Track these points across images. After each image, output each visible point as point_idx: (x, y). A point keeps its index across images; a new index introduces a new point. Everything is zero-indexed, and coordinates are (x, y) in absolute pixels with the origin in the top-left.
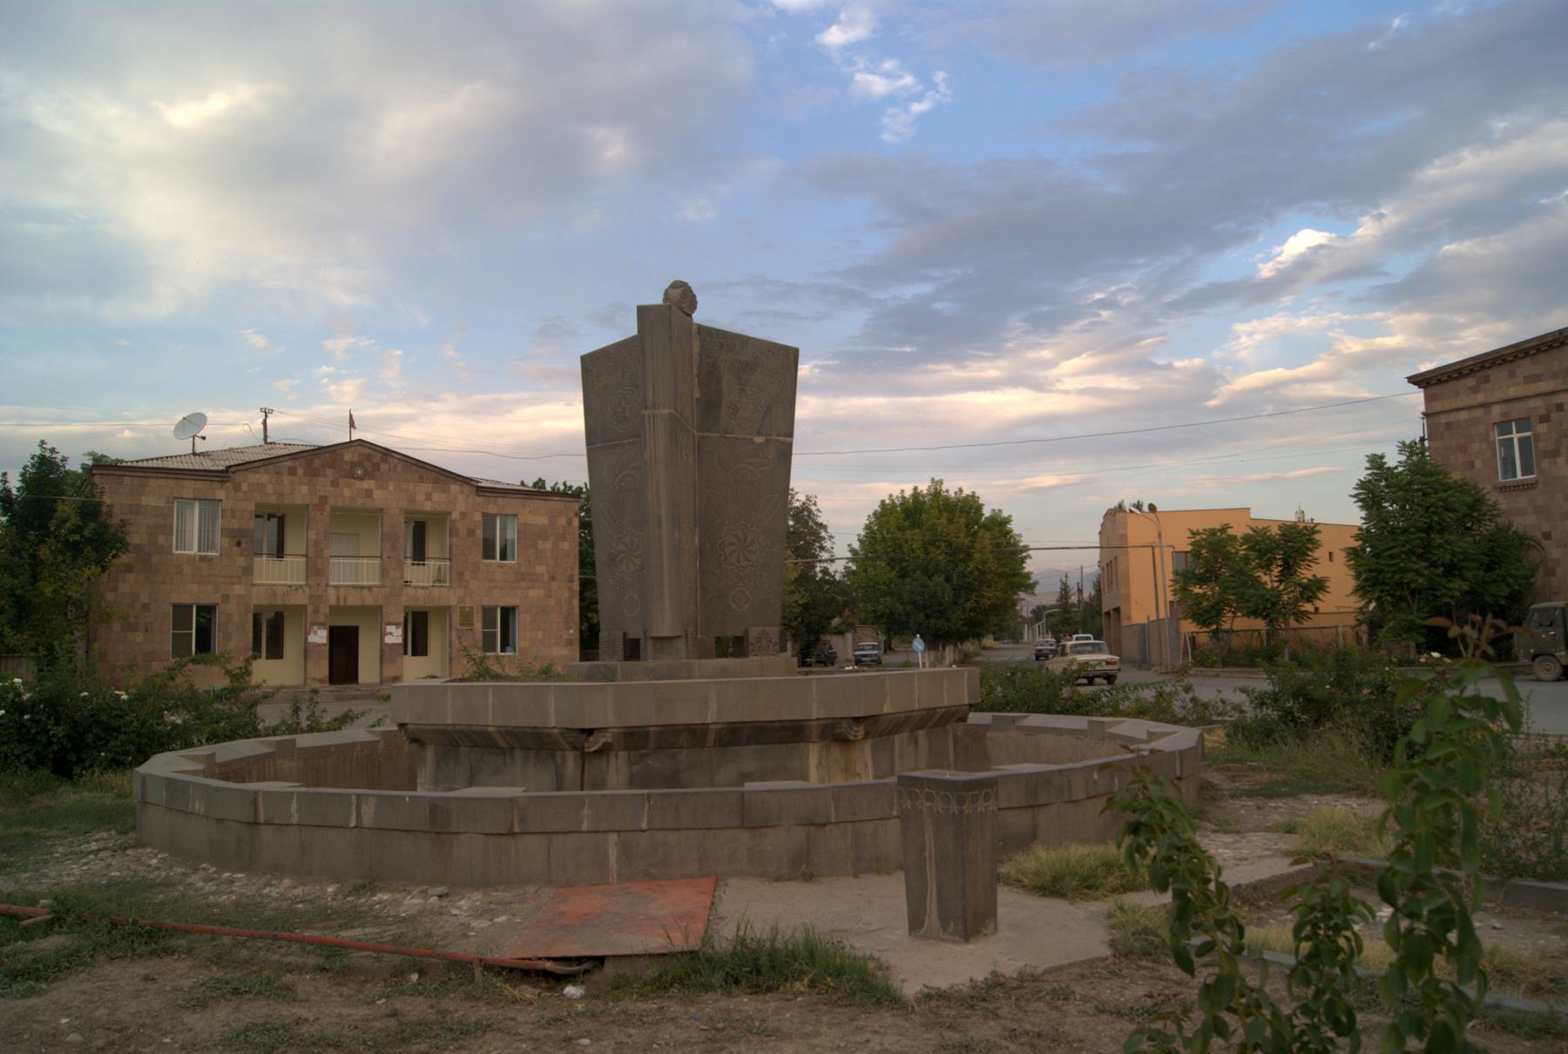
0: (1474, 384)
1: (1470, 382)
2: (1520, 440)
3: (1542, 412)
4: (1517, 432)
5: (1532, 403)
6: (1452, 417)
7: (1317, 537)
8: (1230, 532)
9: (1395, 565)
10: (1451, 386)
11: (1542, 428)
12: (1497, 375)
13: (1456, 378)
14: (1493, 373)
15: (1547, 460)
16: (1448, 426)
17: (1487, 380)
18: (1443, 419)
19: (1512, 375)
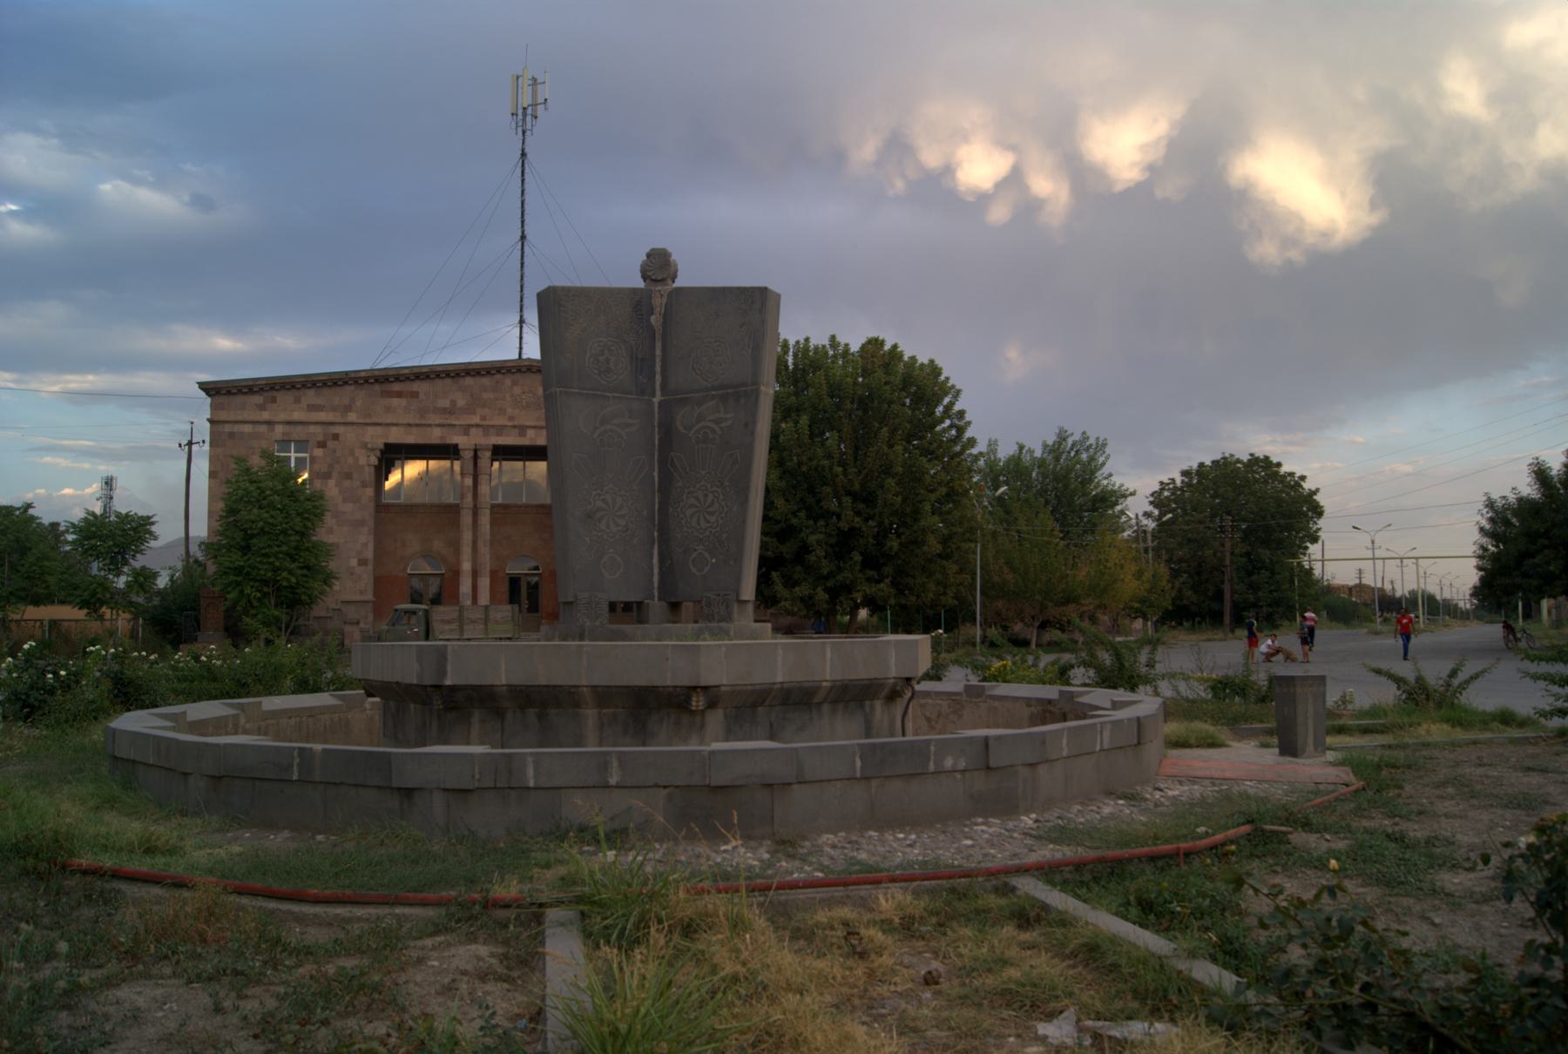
0: (261, 402)
1: (258, 399)
2: (296, 458)
3: (321, 438)
4: (295, 452)
5: (312, 429)
6: (237, 428)
7: (153, 528)
8: (31, 511)
9: (270, 563)
10: (239, 399)
11: (319, 452)
12: (285, 398)
13: (246, 393)
14: (280, 395)
15: (319, 481)
16: (232, 435)
17: (274, 400)
18: (227, 428)
19: (297, 401)
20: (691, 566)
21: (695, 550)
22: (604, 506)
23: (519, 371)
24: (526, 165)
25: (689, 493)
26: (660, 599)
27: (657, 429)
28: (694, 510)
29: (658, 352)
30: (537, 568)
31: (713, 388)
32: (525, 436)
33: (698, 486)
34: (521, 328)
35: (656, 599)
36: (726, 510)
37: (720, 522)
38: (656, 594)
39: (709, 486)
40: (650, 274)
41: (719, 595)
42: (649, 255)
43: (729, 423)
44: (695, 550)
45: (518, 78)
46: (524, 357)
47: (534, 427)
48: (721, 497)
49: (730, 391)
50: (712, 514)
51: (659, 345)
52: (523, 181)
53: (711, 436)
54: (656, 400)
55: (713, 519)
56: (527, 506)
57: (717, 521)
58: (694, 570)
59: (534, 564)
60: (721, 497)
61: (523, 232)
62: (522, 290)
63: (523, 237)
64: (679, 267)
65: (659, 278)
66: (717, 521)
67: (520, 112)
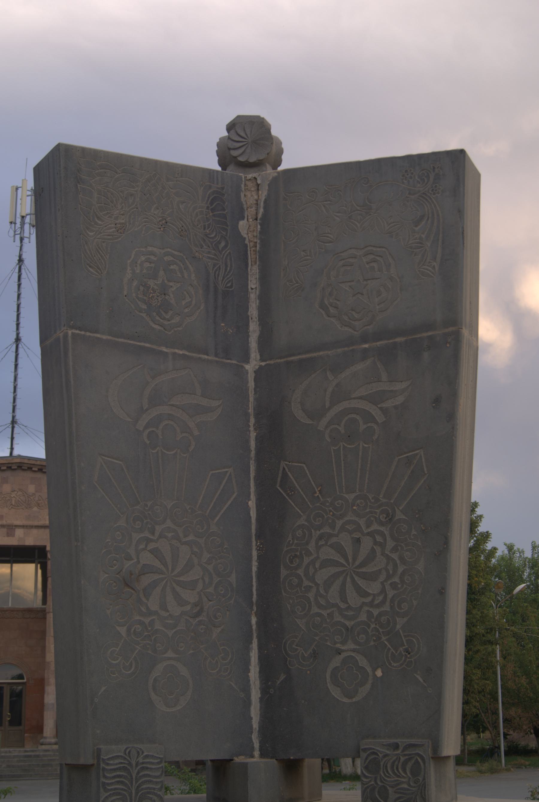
20: (330, 686)
21: (339, 652)
22: (157, 564)
23: (9, 468)
24: (23, 271)
25: (320, 537)
26: (263, 755)
27: (252, 421)
28: (333, 570)
29: (253, 283)
30: (21, 677)
31: (364, 339)
32: (13, 535)
33: (339, 523)
34: (13, 428)
35: (257, 753)
36: (400, 570)
37: (391, 593)
38: (257, 745)
39: (362, 522)
40: (234, 153)
41: (396, 746)
42: (231, 127)
43: (400, 400)
44: (339, 652)
45: (17, 189)
46: (16, 453)
47: (23, 527)
48: (390, 544)
49: (399, 340)
50: (370, 577)
51: (254, 271)
52: (19, 285)
53: (362, 427)
54: (251, 367)
55: (374, 588)
56: (12, 610)
57: (383, 591)
58: (336, 693)
59: (17, 672)
60: (390, 544)
61: (18, 334)
62: (15, 391)
63: (18, 340)
64: (283, 146)
65: (252, 160)
66: (383, 591)
67: (18, 221)
